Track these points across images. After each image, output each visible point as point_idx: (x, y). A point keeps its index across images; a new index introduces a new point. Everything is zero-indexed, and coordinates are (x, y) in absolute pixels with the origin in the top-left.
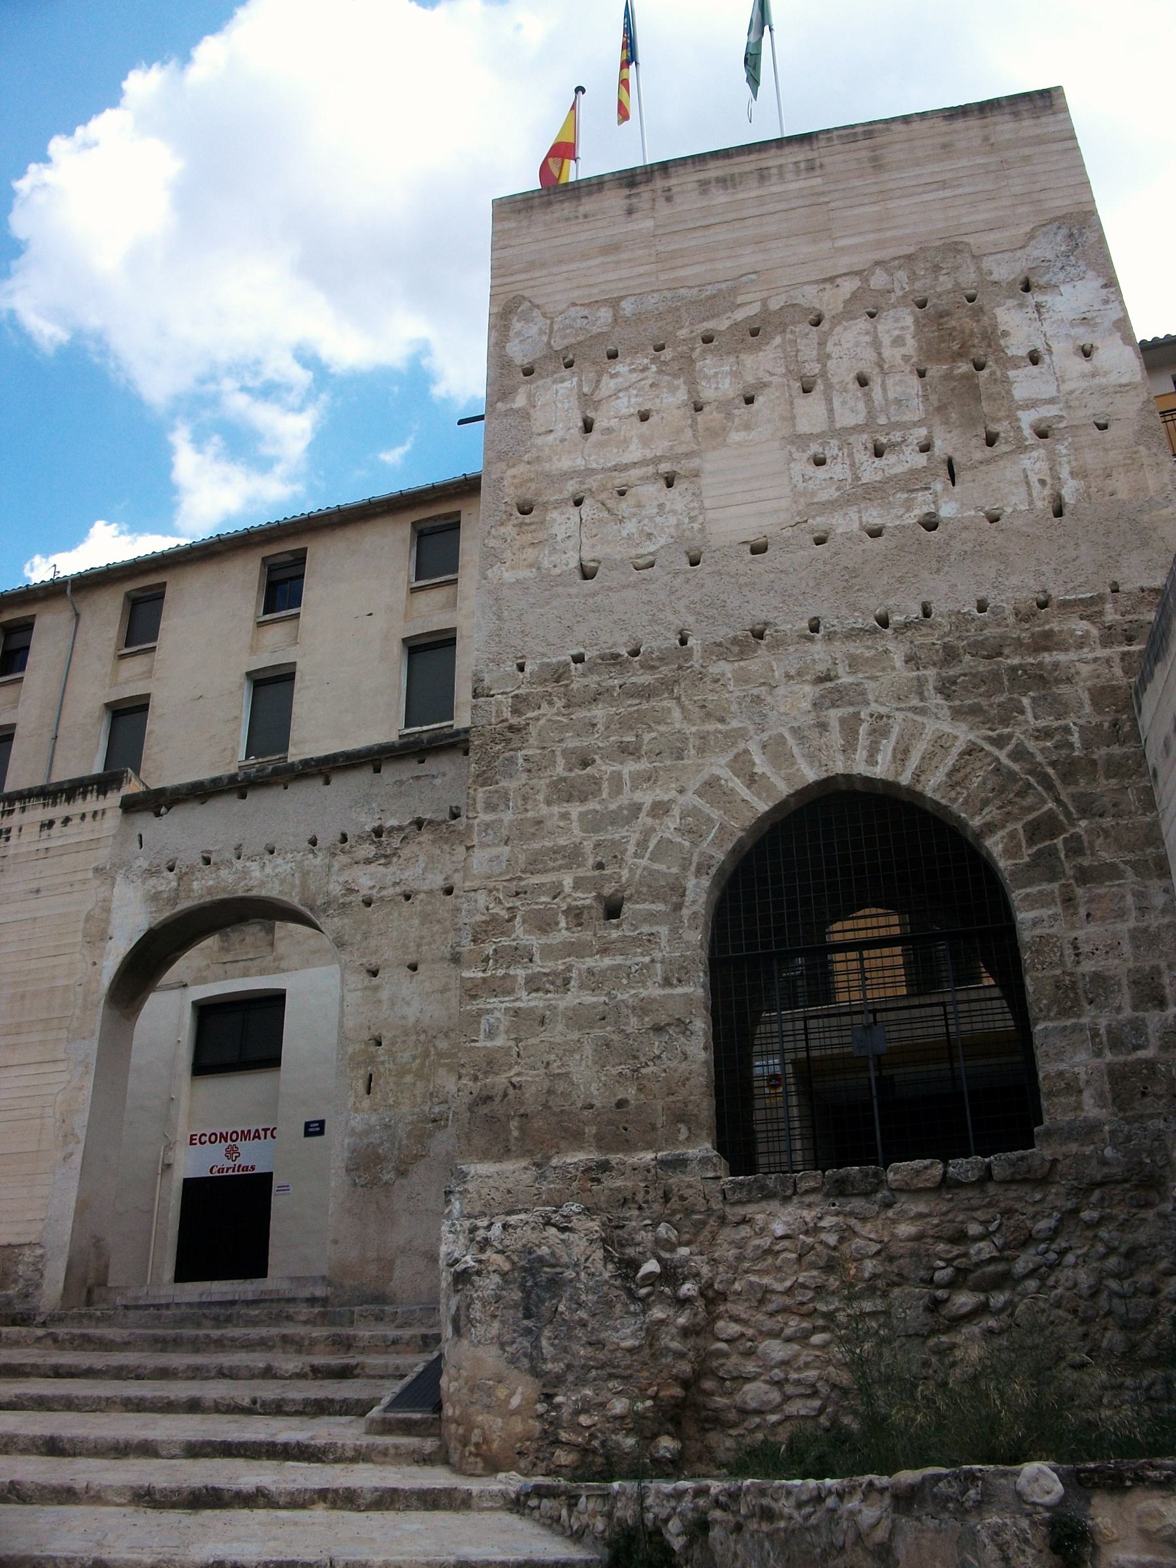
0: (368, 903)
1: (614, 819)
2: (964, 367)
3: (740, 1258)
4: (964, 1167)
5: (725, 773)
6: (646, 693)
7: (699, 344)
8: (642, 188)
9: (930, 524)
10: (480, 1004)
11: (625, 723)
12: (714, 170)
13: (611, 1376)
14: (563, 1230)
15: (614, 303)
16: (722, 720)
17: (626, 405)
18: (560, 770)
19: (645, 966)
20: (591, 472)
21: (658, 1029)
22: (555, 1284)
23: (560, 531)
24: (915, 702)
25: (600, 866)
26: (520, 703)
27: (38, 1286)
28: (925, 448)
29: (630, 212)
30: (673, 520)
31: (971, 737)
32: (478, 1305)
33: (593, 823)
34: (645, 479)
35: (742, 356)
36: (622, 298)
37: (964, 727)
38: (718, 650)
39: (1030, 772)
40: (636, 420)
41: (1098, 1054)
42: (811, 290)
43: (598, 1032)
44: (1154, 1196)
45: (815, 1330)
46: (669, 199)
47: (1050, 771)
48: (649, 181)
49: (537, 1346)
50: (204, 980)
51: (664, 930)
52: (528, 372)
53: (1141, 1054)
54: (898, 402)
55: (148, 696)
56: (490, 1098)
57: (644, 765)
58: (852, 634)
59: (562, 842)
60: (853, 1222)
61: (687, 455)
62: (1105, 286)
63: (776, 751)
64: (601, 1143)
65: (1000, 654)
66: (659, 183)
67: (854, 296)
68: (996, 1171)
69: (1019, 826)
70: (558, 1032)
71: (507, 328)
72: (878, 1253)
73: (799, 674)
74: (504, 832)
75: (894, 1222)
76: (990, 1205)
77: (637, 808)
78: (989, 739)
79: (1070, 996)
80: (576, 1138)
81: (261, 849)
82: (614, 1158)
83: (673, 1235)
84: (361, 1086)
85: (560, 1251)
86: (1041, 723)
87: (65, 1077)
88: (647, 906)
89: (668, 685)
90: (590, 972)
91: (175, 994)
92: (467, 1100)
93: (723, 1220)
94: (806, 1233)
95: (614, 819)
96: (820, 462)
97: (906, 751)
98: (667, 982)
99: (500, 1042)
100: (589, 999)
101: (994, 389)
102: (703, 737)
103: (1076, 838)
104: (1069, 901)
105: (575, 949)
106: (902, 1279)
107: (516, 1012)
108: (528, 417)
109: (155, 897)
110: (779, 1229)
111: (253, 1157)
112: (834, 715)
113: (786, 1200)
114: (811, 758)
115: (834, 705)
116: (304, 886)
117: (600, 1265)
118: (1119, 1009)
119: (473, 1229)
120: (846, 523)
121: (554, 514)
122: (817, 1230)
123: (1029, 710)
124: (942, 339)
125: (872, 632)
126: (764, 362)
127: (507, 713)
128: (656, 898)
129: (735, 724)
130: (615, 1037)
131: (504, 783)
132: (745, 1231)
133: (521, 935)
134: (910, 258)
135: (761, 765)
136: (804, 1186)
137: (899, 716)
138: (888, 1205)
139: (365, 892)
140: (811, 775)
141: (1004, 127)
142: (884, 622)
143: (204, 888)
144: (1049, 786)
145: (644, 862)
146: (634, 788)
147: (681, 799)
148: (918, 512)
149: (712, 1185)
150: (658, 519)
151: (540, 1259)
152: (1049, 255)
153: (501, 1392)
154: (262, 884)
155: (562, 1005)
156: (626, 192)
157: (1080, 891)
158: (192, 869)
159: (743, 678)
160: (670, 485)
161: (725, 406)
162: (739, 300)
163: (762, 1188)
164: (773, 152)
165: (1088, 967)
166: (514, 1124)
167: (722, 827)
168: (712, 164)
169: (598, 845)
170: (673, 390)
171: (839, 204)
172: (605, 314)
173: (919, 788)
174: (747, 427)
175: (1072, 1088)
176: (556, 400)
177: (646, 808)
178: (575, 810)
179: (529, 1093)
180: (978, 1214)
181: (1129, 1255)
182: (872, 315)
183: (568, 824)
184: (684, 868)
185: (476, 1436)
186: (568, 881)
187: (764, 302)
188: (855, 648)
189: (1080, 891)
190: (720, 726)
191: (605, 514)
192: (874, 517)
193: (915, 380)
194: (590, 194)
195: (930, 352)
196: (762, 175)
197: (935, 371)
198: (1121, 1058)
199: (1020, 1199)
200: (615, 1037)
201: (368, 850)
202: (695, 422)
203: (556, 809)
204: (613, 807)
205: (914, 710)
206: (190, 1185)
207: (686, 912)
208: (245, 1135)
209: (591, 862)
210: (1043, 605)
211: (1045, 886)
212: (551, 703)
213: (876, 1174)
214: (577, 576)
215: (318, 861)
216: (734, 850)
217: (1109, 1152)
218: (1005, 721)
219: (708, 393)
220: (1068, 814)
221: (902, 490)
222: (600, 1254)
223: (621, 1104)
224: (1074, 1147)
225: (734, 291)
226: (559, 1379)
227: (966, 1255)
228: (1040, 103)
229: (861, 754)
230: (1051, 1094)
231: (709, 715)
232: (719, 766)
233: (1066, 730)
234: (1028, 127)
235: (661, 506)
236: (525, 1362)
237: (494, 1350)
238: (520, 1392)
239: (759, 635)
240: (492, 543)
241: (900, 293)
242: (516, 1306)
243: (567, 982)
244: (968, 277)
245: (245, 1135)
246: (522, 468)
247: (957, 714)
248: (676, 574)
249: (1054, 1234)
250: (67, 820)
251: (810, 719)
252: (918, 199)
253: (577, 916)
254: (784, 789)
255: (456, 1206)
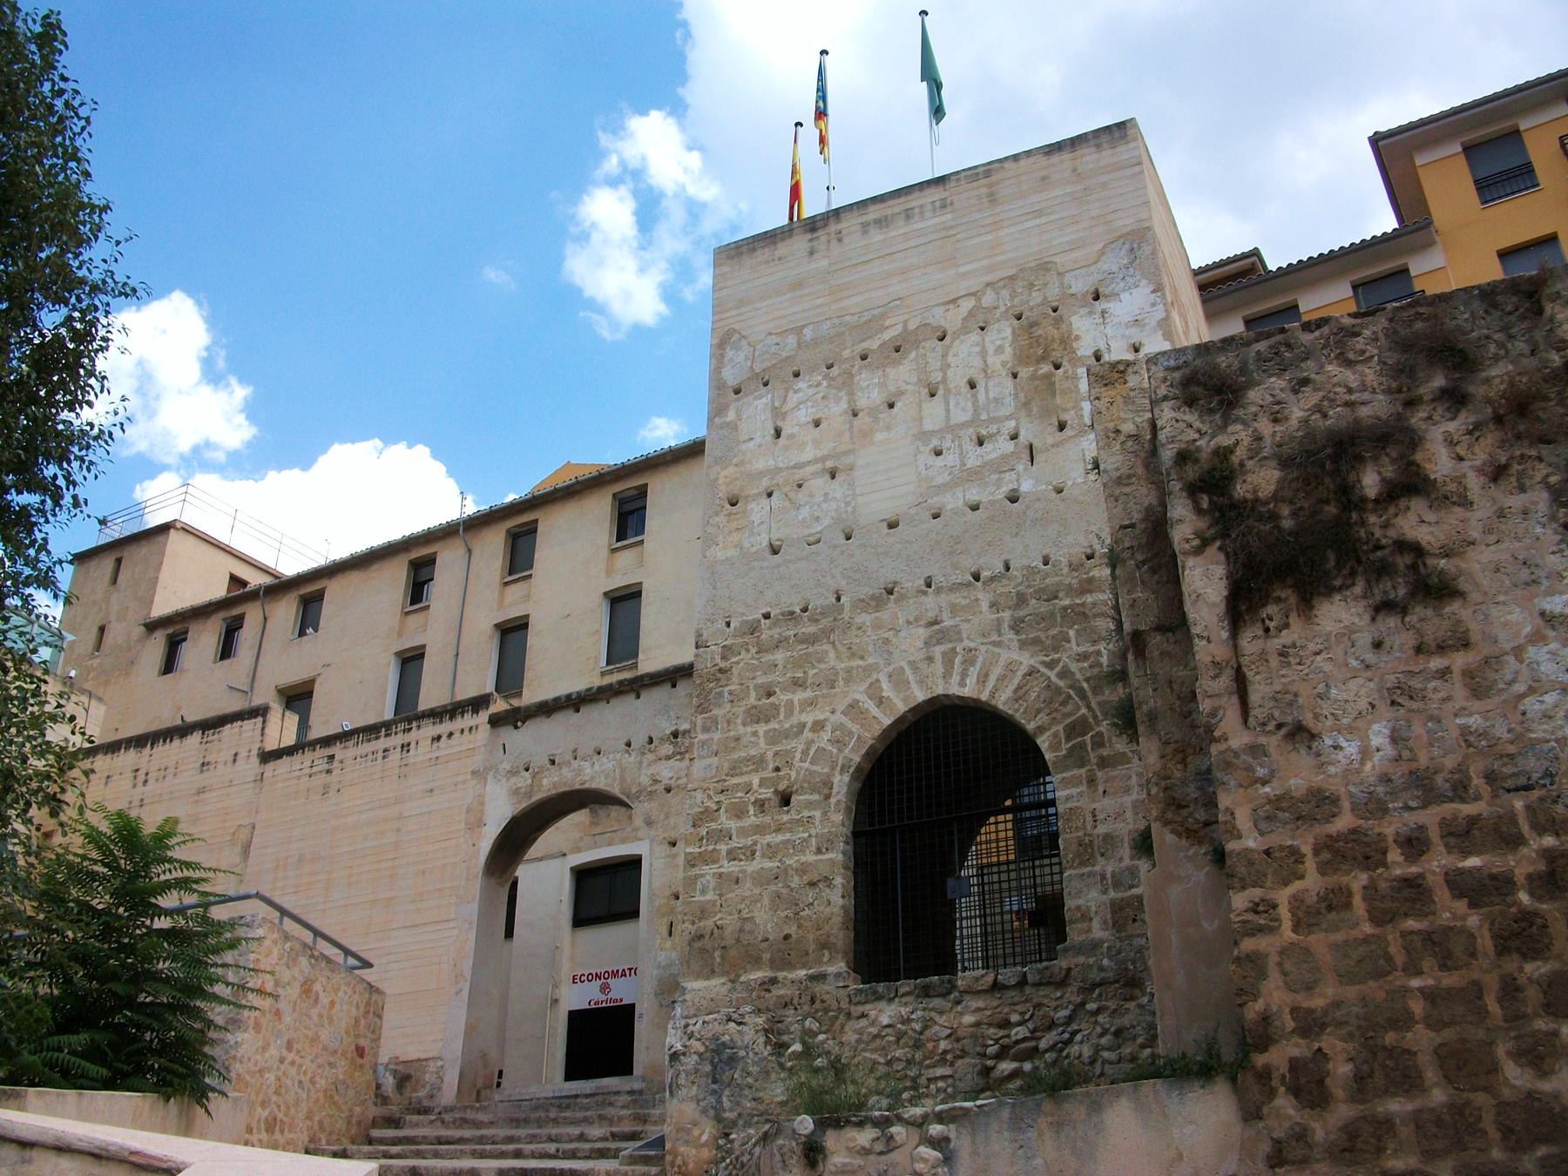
0: (668, 790)
1: (786, 735)
2: (1046, 368)
3: (859, 1041)
4: (1008, 975)
5: (862, 697)
6: (811, 640)
7: (858, 361)
8: (820, 233)
9: (1013, 499)
10: (696, 871)
11: (797, 663)
12: (874, 212)
13: (767, 1121)
14: (740, 1024)
15: (798, 331)
16: (862, 658)
17: (804, 415)
18: (752, 700)
19: (805, 840)
20: (778, 470)
21: (812, 884)
22: (732, 1061)
23: (756, 518)
24: (995, 638)
25: (777, 769)
26: (727, 651)
27: (439, 1089)
28: (1014, 437)
29: (811, 253)
30: (834, 506)
31: (1032, 662)
32: (683, 1075)
33: (773, 738)
34: (815, 474)
35: (888, 370)
36: (804, 326)
37: (1026, 654)
38: (862, 605)
39: (1071, 687)
40: (811, 426)
41: (1105, 892)
42: (939, 311)
43: (773, 888)
44: (1137, 992)
45: (906, 1089)
46: (840, 240)
47: (1085, 685)
48: (826, 225)
49: (719, 1101)
50: (578, 850)
51: (817, 814)
52: (737, 392)
53: (1135, 891)
54: (996, 400)
55: (527, 616)
56: (702, 936)
57: (808, 694)
58: (955, 588)
59: (753, 752)
60: (933, 1014)
61: (845, 453)
62: (1154, 291)
63: (897, 679)
64: (774, 964)
65: (1056, 597)
66: (833, 227)
67: (971, 314)
68: (1029, 977)
69: (1060, 728)
70: (747, 888)
71: (722, 356)
72: (949, 1036)
73: (916, 620)
74: (715, 747)
75: (962, 1014)
76: (1026, 1001)
77: (803, 725)
78: (1044, 663)
79: (1088, 851)
80: (756, 962)
81: (591, 752)
82: (781, 975)
83: (815, 1026)
84: (664, 930)
85: (736, 1037)
86: (1081, 649)
87: (456, 932)
88: (807, 797)
89: (827, 633)
90: (769, 845)
91: (556, 862)
92: (688, 937)
93: (849, 1015)
94: (903, 1023)
95: (786, 735)
96: (938, 453)
97: (986, 675)
98: (819, 851)
99: (710, 896)
100: (768, 864)
101: (1066, 385)
102: (849, 671)
103: (1100, 734)
104: (1091, 781)
105: (760, 830)
106: (963, 1054)
107: (720, 875)
108: (736, 428)
109: (516, 792)
110: (885, 1020)
111: (621, 991)
112: (938, 651)
113: (891, 1000)
114: (921, 682)
115: (939, 643)
116: (623, 779)
117: (762, 1047)
118: (1121, 859)
119: (687, 1026)
120: (953, 501)
121: (753, 505)
122: (909, 1021)
123: (1073, 640)
124: (1031, 346)
125: (969, 585)
126: (903, 374)
127: (718, 660)
128: (813, 790)
129: (871, 660)
130: (784, 891)
131: (715, 712)
132: (863, 1022)
133: (725, 821)
134: (1012, 278)
135: (887, 690)
136: (902, 991)
137: (983, 648)
138: (958, 1003)
139: (665, 781)
140: (920, 696)
141: (1088, 158)
142: (977, 577)
143: (551, 783)
144: (1082, 695)
145: (807, 765)
146: (802, 711)
147: (833, 718)
148: (1005, 489)
149: (843, 993)
150: (824, 506)
151: (724, 1044)
152: (1114, 269)
153: (696, 1132)
154: (593, 778)
155: (750, 869)
156: (809, 236)
157: (1099, 774)
158: (542, 768)
159: (877, 626)
160: (833, 477)
161: (873, 412)
162: (887, 323)
163: (875, 992)
164: (916, 194)
165: (1101, 829)
166: (717, 954)
167: (859, 737)
168: (872, 208)
169: (776, 754)
170: (838, 400)
171: (963, 235)
172: (792, 340)
173: (993, 702)
174: (888, 428)
175: (1086, 917)
176: (755, 412)
177: (809, 725)
178: (762, 728)
179: (728, 931)
180: (1019, 1008)
181: (1118, 1033)
182: (982, 329)
183: (756, 739)
184: (833, 768)
185: (679, 1161)
186: (756, 781)
187: (905, 326)
188: (958, 599)
189: (1099, 774)
190: (861, 663)
191: (787, 503)
192: (974, 495)
193: (1009, 382)
194: (783, 239)
195: (1022, 358)
196: (908, 215)
197: (1024, 373)
198: (1120, 895)
199: (1046, 996)
200: (784, 891)
201: (667, 749)
202: (852, 426)
203: (749, 729)
204: (787, 726)
205: (994, 643)
206: (574, 1016)
207: (833, 800)
208: (615, 974)
209: (771, 766)
210: (1089, 557)
211: (1076, 772)
212: (747, 651)
213: (950, 982)
214: (768, 551)
215: (632, 759)
216: (867, 753)
217: (1105, 962)
218: (1056, 649)
219: (862, 402)
220: (1095, 717)
221: (995, 472)
222: (762, 1039)
223: (787, 937)
224: (1082, 959)
225: (883, 316)
226: (734, 1123)
227: (1008, 1036)
228: (1117, 135)
229: (956, 679)
230: (1072, 922)
231: (853, 655)
232: (858, 693)
233: (1099, 653)
234: (1107, 156)
235: (826, 495)
236: (712, 1112)
237: (693, 1105)
238: (707, 1132)
239: (890, 592)
240: (710, 530)
241: (1003, 309)
242: (707, 1075)
243: (753, 853)
244: (1053, 293)
245: (615, 974)
246: (731, 470)
247: (1023, 645)
248: (835, 547)
249: (1070, 1019)
250: (451, 734)
251: (922, 655)
252: (1021, 227)
253: (761, 805)
254: (901, 707)
255: (678, 1010)
